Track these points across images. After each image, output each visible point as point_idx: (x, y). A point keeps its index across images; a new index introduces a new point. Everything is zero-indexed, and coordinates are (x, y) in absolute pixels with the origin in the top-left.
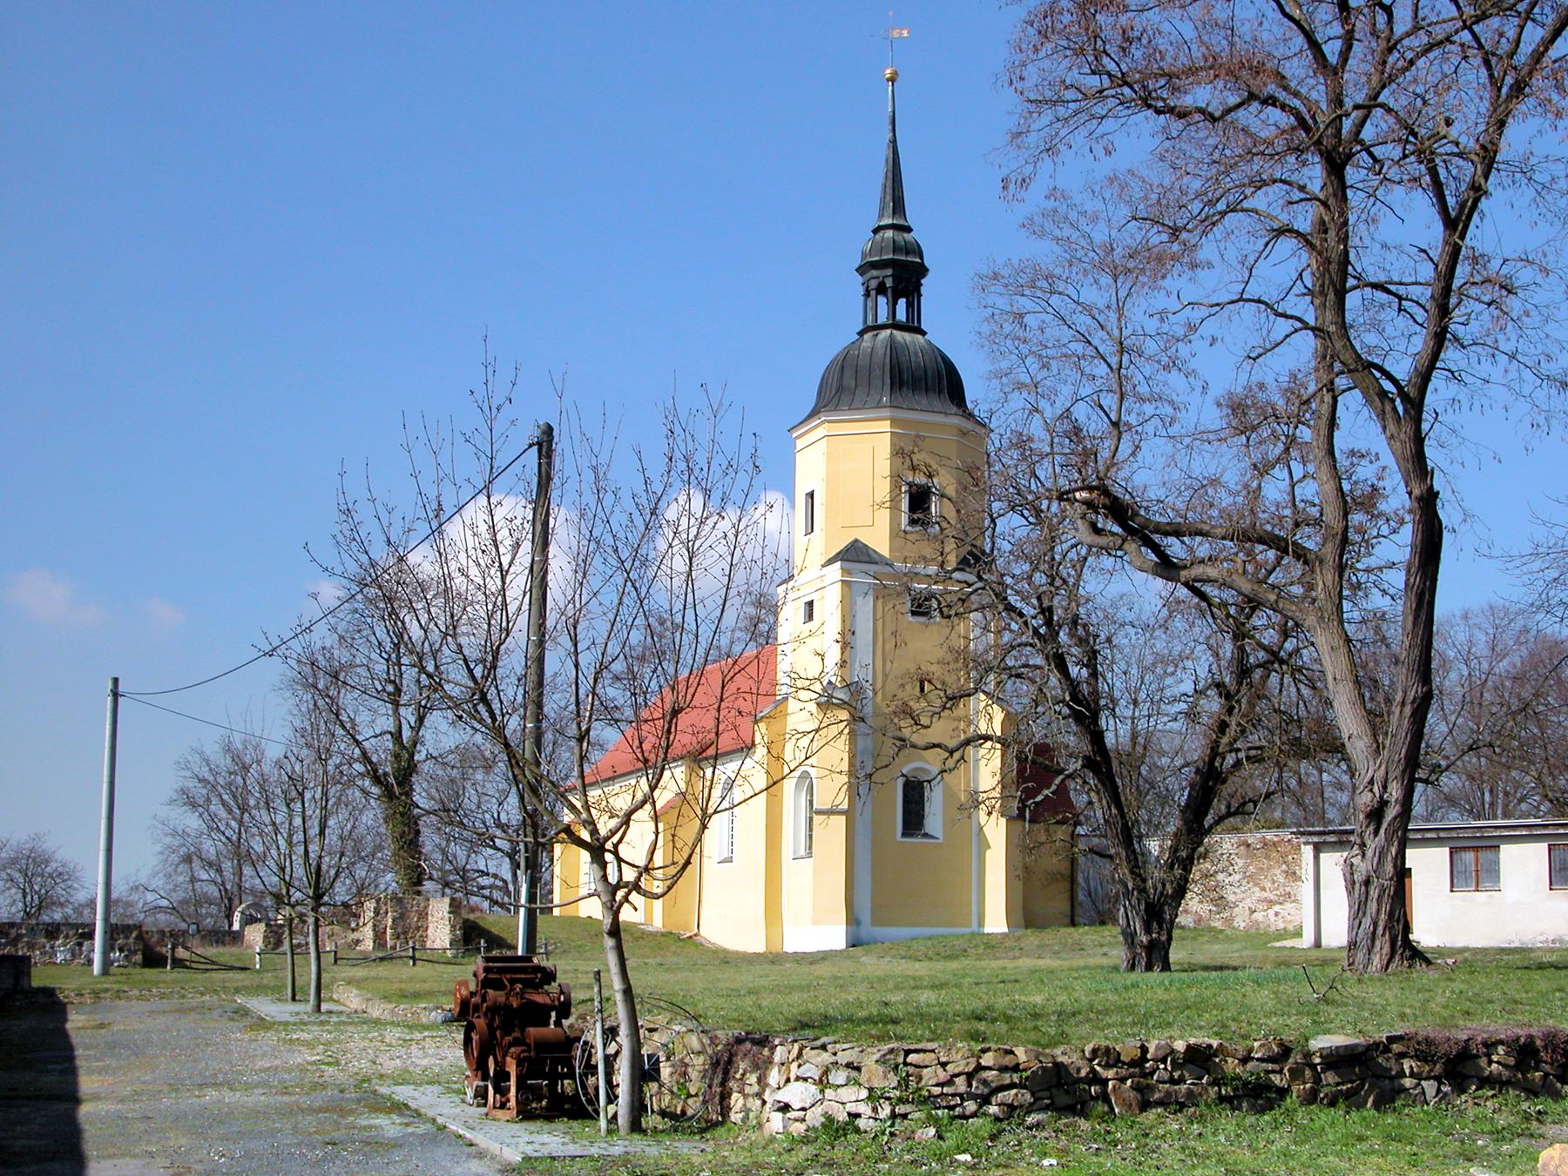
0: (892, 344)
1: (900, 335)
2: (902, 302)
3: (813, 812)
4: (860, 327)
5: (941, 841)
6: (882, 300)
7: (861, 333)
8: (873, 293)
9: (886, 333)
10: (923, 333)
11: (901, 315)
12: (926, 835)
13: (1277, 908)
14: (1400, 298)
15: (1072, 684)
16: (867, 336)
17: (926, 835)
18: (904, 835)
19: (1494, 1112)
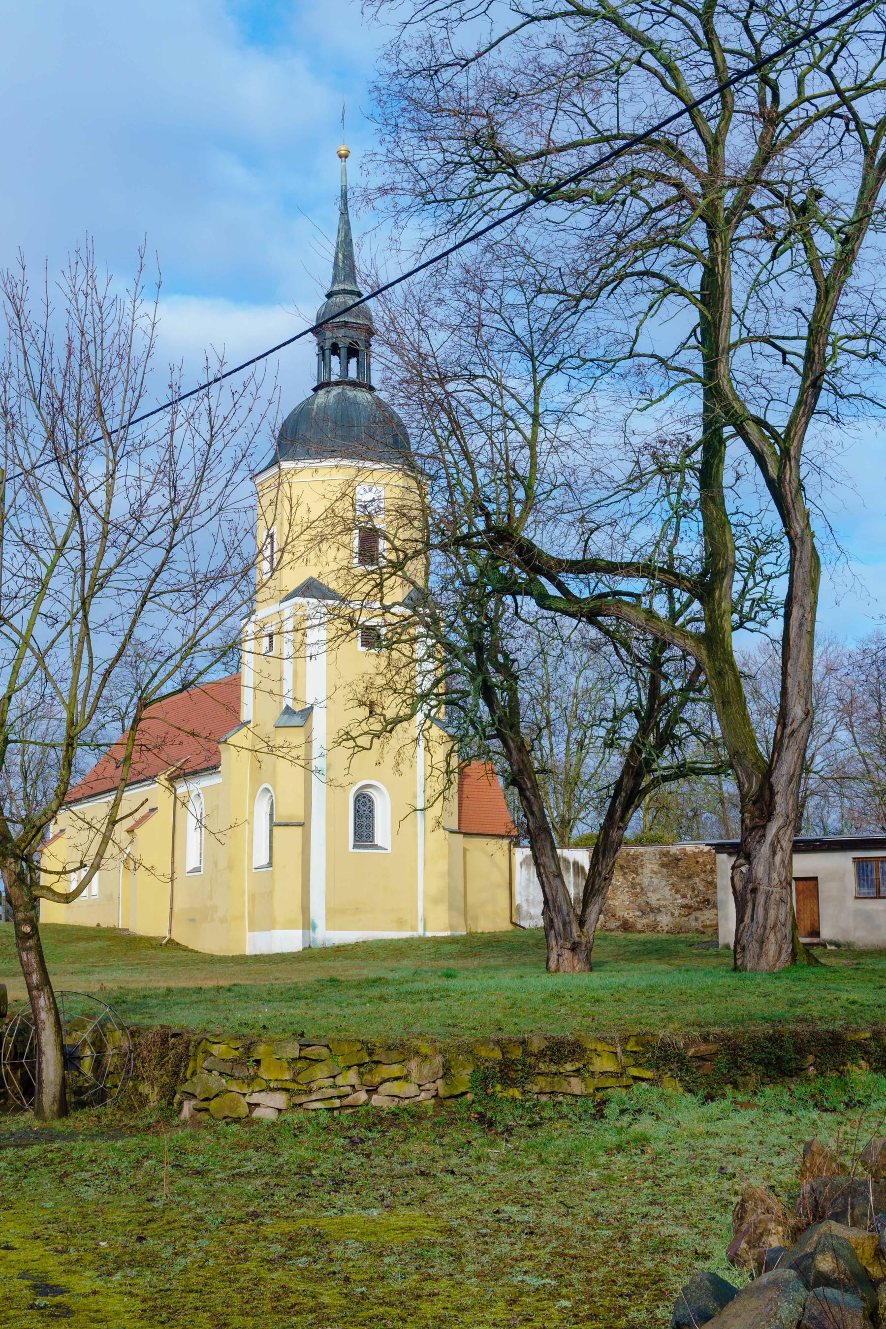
0: (341, 398)
1: (351, 393)
2: (353, 361)
3: (303, 825)
4: (315, 384)
5: (389, 851)
6: (335, 360)
7: (315, 390)
8: (327, 352)
9: (336, 391)
10: (371, 389)
11: (353, 374)
12: (376, 847)
13: (698, 914)
14: (784, 353)
15: (183, 659)
16: (321, 392)
17: (376, 847)
18: (355, 846)
19: (181, 1151)
